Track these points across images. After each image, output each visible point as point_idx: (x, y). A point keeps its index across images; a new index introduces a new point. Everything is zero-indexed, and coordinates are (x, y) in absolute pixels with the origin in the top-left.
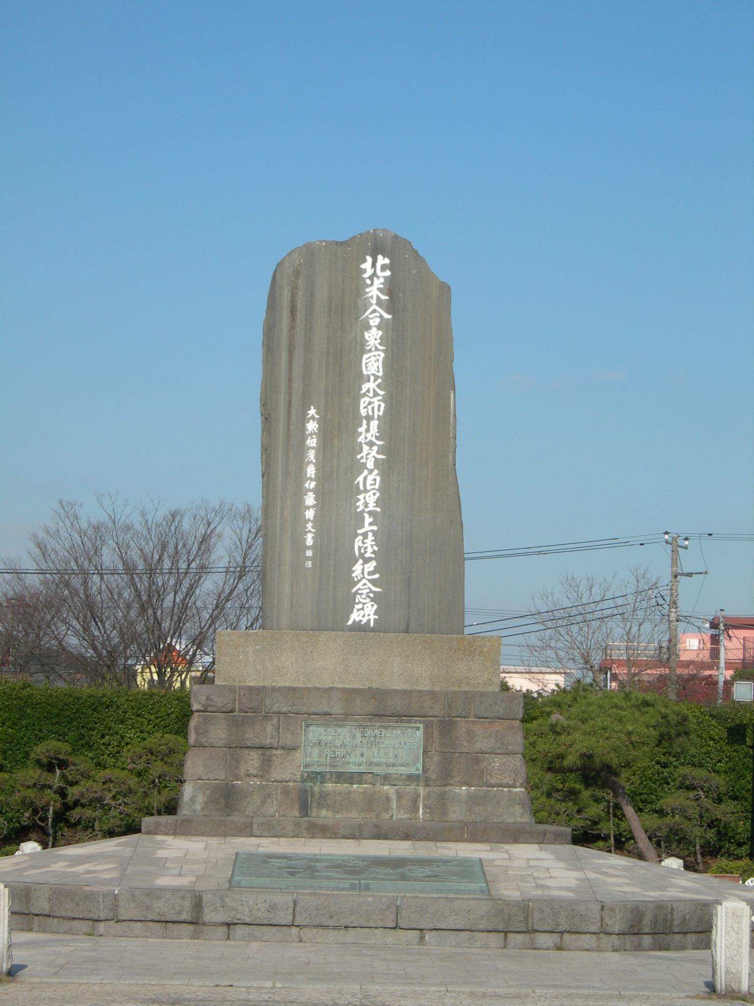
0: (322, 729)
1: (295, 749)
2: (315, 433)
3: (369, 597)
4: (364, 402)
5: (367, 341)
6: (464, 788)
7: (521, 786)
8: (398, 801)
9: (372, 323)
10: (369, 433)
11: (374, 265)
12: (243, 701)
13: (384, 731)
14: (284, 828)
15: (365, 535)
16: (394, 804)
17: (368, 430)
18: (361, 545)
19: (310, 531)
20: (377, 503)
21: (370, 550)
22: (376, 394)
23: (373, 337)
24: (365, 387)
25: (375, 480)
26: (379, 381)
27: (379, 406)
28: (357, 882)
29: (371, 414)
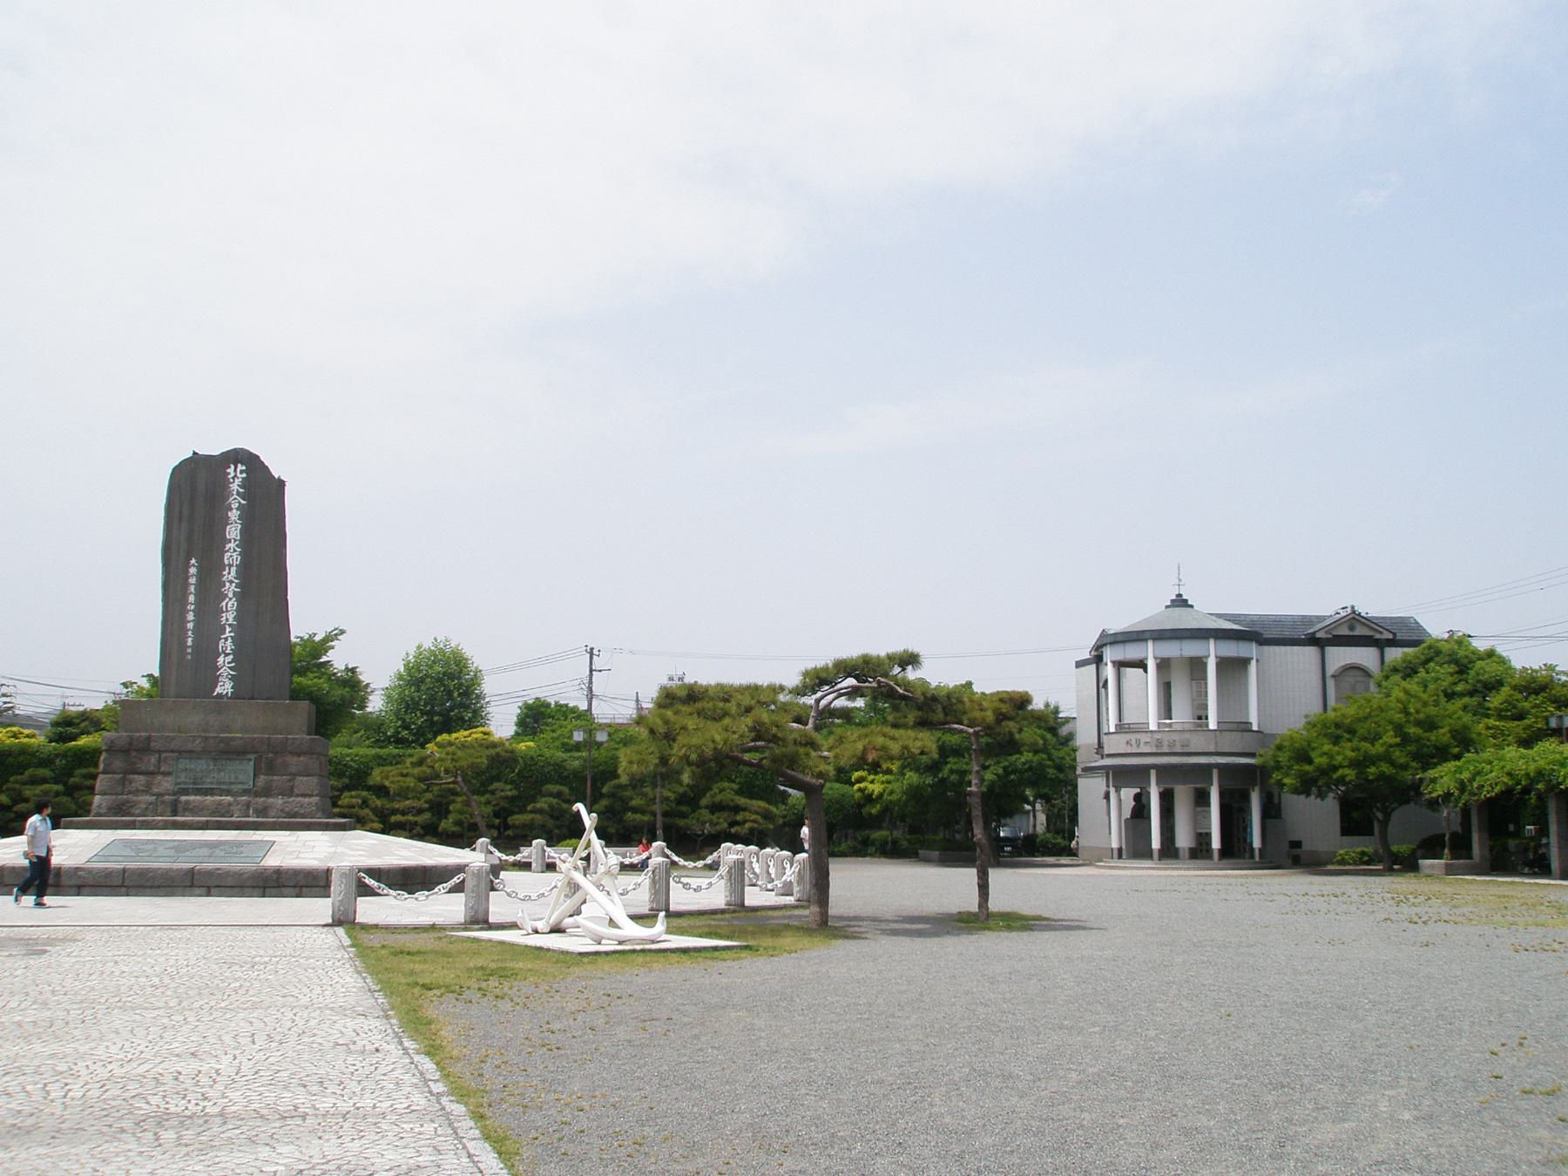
4: (227, 555)
10: (230, 574)
23: (234, 515)
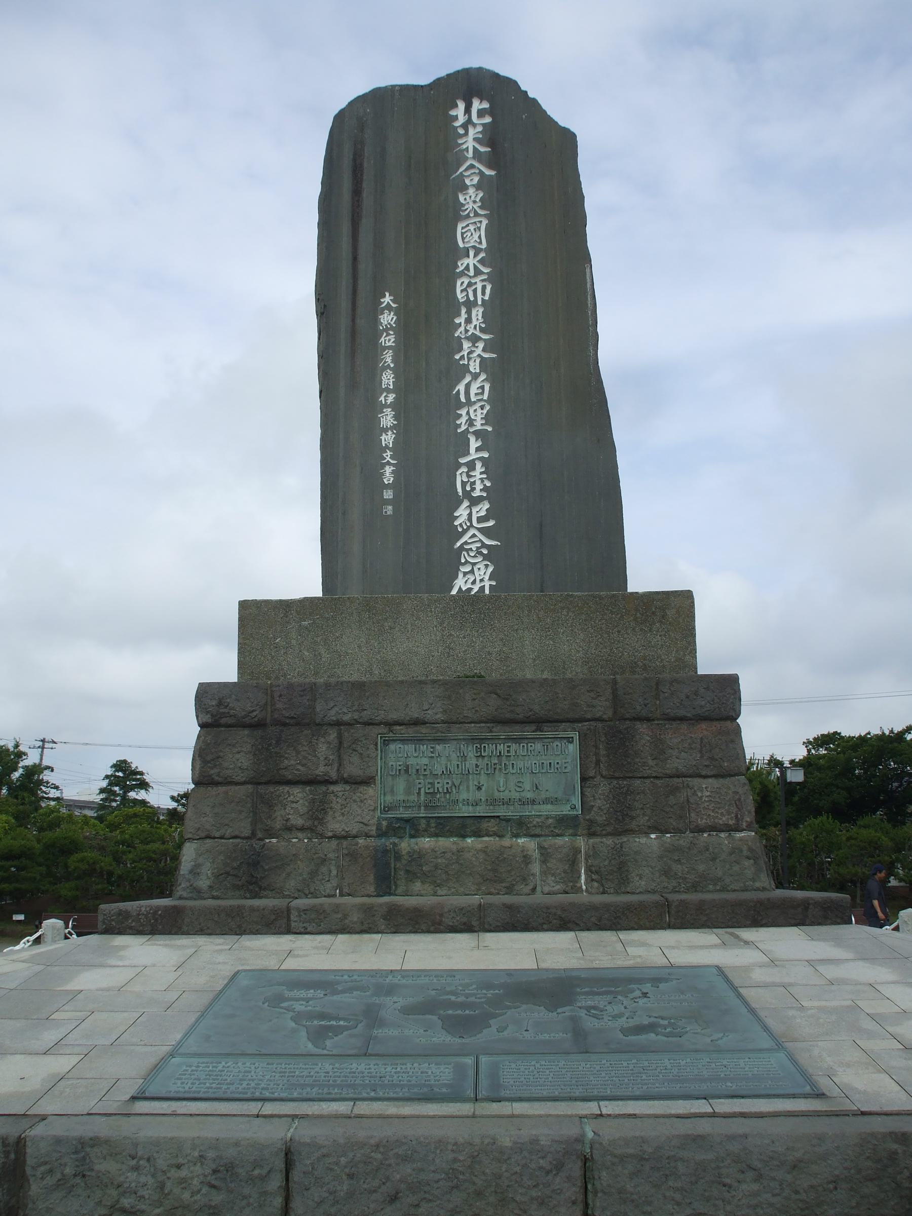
0: (410, 748)
1: (368, 781)
2: (392, 328)
3: (481, 553)
4: (460, 284)
5: (463, 205)
6: (653, 836)
7: (749, 828)
8: (544, 862)
9: (468, 182)
10: (470, 324)
11: (468, 110)
12: (279, 705)
13: (514, 746)
14: (345, 916)
15: (471, 466)
16: (536, 868)
17: (468, 320)
18: (465, 479)
19: (388, 463)
20: (487, 419)
21: (479, 486)
22: (478, 272)
23: (471, 199)
24: (461, 265)
25: (482, 388)
26: (482, 255)
27: (484, 288)
28: (469, 1061)
29: (472, 299)
